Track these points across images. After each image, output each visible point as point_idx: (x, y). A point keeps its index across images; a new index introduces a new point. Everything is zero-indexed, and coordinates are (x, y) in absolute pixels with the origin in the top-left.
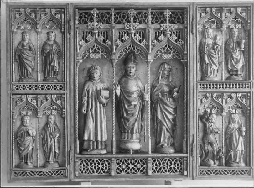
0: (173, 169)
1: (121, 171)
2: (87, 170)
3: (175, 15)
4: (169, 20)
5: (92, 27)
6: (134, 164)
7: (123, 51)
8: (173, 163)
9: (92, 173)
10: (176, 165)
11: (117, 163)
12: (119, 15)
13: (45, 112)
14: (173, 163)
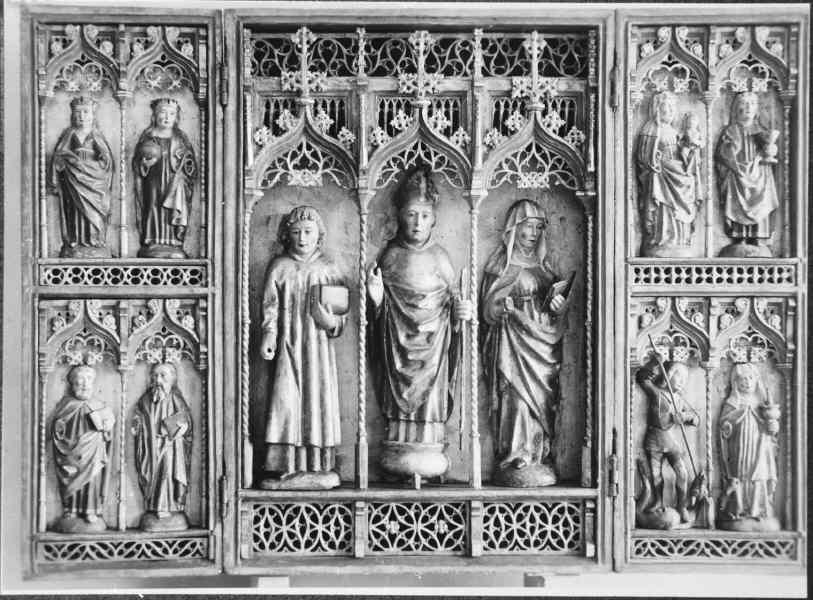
0: (549, 536)
2: (279, 537)
4: (540, 65)
14: (550, 519)
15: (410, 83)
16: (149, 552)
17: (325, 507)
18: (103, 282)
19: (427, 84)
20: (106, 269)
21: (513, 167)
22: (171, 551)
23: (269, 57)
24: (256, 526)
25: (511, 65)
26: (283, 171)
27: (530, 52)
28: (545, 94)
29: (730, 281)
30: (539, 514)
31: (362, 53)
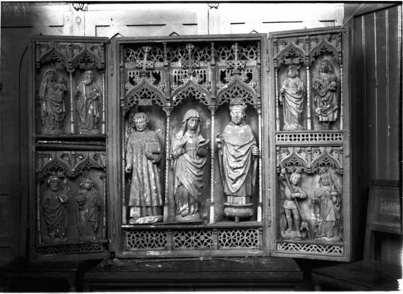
0: (245, 241)
1: (145, 245)
5: (186, 65)
10: (250, 236)
13: (318, 170)
16: (322, 247)
19: (147, 65)
22: (302, 249)
29: (307, 139)
31: (236, 54)
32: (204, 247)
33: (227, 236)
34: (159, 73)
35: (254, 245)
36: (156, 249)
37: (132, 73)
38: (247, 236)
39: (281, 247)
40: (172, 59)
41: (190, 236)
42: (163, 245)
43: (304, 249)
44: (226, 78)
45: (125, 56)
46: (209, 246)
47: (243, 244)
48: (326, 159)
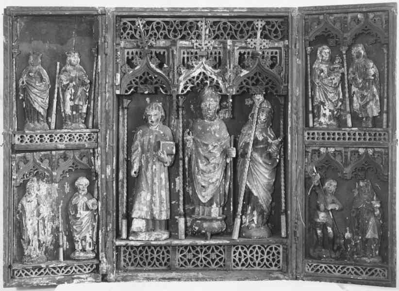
0: (265, 261)
1: (144, 264)
2: (262, 260)
3: (270, 26)
4: (261, 34)
6: (205, 252)
7: (188, 82)
8: (266, 253)
9: (252, 265)
10: (271, 255)
11: (180, 251)
12: (217, 26)
14: (266, 253)
15: (252, 43)
16: (362, 270)
17: (268, 247)
18: (84, 140)
19: (261, 44)
20: (75, 134)
21: (247, 84)
23: (196, 30)
24: (168, 258)
25: (181, 34)
26: (135, 86)
27: (257, 26)
28: (208, 48)
30: (260, 251)
32: (216, 267)
33: (243, 254)
34: (164, 53)
35: (276, 265)
36: (157, 268)
37: (130, 53)
38: (153, 257)
39: (310, 269)
40: (180, 36)
41: (199, 254)
42: (165, 264)
43: (339, 271)
44: (246, 62)
45: (122, 31)
46: (221, 266)
47: (262, 264)
48: (327, 161)
